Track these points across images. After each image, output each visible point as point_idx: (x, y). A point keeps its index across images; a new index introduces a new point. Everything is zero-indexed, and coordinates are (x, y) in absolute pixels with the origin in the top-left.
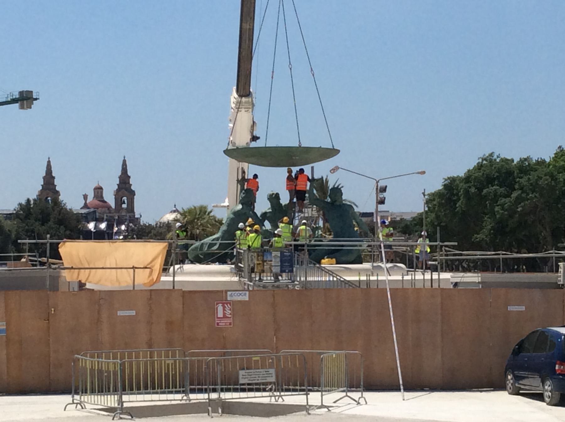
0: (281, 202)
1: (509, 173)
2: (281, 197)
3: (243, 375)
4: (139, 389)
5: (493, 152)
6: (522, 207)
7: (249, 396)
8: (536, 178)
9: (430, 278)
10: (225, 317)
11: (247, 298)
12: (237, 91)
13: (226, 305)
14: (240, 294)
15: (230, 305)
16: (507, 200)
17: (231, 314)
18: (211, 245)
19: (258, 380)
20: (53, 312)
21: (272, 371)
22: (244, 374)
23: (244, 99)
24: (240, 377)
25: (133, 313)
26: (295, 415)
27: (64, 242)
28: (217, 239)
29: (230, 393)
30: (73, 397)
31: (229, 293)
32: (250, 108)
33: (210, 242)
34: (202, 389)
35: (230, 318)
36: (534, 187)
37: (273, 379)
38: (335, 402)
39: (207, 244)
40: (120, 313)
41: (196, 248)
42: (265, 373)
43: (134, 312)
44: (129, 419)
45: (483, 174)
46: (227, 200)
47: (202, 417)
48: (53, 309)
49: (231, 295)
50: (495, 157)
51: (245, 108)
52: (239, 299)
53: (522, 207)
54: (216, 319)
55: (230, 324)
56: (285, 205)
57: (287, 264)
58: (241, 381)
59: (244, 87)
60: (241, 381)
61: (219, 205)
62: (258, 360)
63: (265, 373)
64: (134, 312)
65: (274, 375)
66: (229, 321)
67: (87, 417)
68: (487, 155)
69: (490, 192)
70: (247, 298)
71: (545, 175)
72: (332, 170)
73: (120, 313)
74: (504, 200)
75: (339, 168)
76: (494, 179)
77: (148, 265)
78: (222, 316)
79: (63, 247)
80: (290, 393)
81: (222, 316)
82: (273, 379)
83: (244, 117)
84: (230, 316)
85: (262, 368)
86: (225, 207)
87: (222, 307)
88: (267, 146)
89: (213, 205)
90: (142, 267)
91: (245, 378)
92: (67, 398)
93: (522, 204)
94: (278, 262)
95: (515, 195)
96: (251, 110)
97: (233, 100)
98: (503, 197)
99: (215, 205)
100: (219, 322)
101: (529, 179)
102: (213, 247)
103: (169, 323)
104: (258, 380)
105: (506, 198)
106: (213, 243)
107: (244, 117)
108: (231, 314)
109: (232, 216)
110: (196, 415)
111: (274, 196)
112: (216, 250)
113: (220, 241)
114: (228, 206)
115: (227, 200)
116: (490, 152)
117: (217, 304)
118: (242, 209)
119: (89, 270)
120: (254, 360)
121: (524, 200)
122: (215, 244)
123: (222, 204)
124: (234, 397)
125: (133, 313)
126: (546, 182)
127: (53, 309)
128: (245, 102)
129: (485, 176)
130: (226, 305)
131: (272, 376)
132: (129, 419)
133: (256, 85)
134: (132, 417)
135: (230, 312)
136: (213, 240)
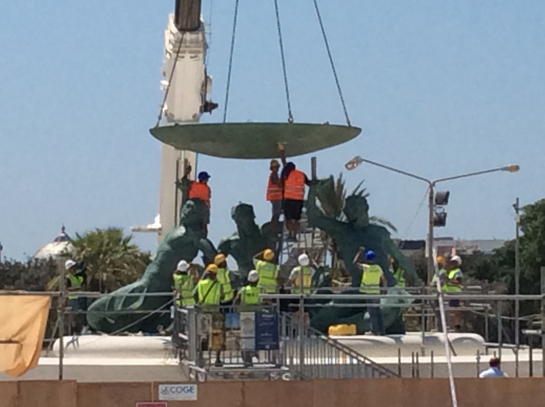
11: (193, 396)
12: (177, 22)
14: (183, 389)
18: (129, 300)
23: (188, 36)
28: (140, 289)
31: (161, 387)
32: (199, 52)
33: (127, 294)
39: (121, 297)
41: (103, 305)
46: (157, 219)
49: (165, 391)
51: (190, 52)
57: (267, 334)
61: (143, 227)
70: (193, 396)
72: (350, 163)
77: (15, 336)
83: (189, 69)
89: (132, 228)
94: (251, 332)
96: (201, 56)
107: (189, 69)
113: (144, 294)
114: (160, 229)
115: (157, 219)
118: (185, 234)
122: (137, 298)
123: (149, 227)
128: (191, 42)
136: (133, 291)
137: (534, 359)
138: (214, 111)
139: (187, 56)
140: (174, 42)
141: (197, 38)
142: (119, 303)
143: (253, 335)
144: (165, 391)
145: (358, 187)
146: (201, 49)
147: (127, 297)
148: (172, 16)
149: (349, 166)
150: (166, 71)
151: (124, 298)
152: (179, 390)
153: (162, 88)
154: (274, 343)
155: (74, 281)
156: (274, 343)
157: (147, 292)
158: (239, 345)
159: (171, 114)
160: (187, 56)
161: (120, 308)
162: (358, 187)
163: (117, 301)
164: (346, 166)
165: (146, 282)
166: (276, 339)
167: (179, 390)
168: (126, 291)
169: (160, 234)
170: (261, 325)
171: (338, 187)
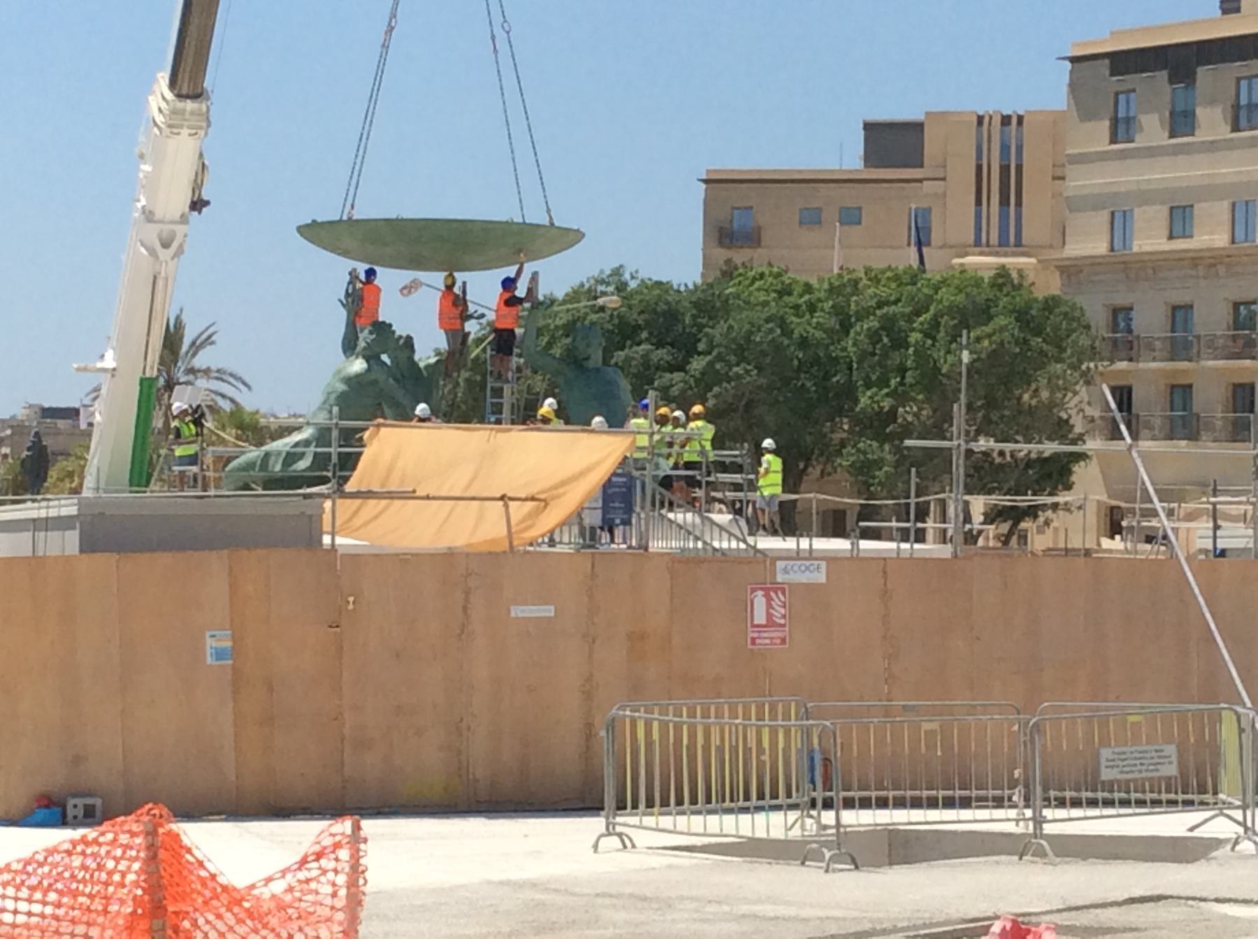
0: (416, 358)
1: (672, 315)
2: (416, 347)
3: (1108, 760)
4: (680, 802)
5: (621, 266)
6: (715, 396)
7: (962, 818)
8: (747, 327)
9: (807, 547)
10: (770, 622)
11: (822, 578)
12: (173, 84)
13: (772, 594)
14: (807, 568)
15: (784, 594)
16: (678, 376)
17: (784, 617)
18: (291, 458)
19: (1140, 771)
20: (351, 607)
21: (1171, 750)
22: (1111, 757)
23: (190, 105)
24: (1103, 763)
25: (548, 611)
26: (945, 865)
27: (379, 426)
28: (307, 443)
29: (854, 812)
30: (607, 818)
31: (780, 565)
32: (200, 128)
33: (287, 449)
34: (853, 799)
35: (784, 626)
36: (742, 350)
37: (1171, 770)
38: (1191, 829)
39: (279, 453)
40: (517, 612)
41: (250, 466)
42: (1154, 754)
43: (552, 608)
44: (849, 870)
45: (612, 316)
46: (110, 354)
47: (997, 863)
48: (351, 599)
49: (785, 571)
50: (627, 276)
51: (189, 127)
52: (805, 581)
53: (715, 396)
54: (750, 629)
55: (783, 641)
56: (428, 367)
57: (617, 505)
58: (1106, 775)
59: (188, 71)
60: (1106, 775)
61: (91, 365)
62: (1139, 723)
63: (1154, 754)
64: (552, 608)
65: (1174, 759)
66: (780, 634)
67: (697, 865)
68: (608, 272)
69: (633, 358)
70: (822, 578)
71: (767, 321)
72: (405, 288)
73: (517, 612)
74: (668, 375)
75: (422, 284)
76: (637, 328)
77: (543, 492)
78: (763, 622)
79: (375, 442)
80: (1129, 811)
81: (763, 622)
82: (1171, 770)
83: (183, 148)
84: (782, 621)
85: (1147, 743)
86: (104, 370)
87: (764, 599)
88: (357, 216)
89: (75, 366)
90: (523, 496)
91: (1112, 767)
92: (593, 825)
93: (716, 389)
94: (596, 501)
95: (697, 364)
96: (202, 133)
97: (154, 102)
98: (664, 371)
99: (83, 365)
100: (756, 635)
101: (730, 327)
102: (295, 462)
103: (636, 638)
104: (1140, 771)
105: (671, 372)
106: (295, 454)
107: (183, 148)
108: (784, 617)
109: (342, 387)
110: (963, 860)
111: (402, 342)
112: (304, 471)
113: (312, 449)
114: (114, 369)
115: (110, 354)
116: (617, 265)
117: (753, 590)
118: (369, 370)
119: (452, 502)
120: (1132, 723)
121: (719, 379)
122: (302, 455)
123: (99, 365)
124: (913, 820)
125: (548, 611)
126: (770, 337)
127: (351, 599)
128: (192, 113)
129: (616, 321)
130: (772, 594)
131: (1171, 763)
132: (849, 870)
133: (218, 74)
134: (857, 867)
135: (783, 611)
136: (297, 445)
137: (801, 547)
138: (204, 210)
139: (185, 132)
140: (166, 112)
141: (200, 109)
142: (276, 462)
143: (600, 505)
144: (785, 571)
145: (207, 329)
146: (204, 124)
147: (288, 453)
148: (163, 78)
149: (405, 292)
150: (144, 151)
151: (284, 455)
152: (796, 568)
153: (141, 175)
154: (625, 516)
155: (185, 431)
156: (625, 516)
157: (317, 446)
158: (581, 519)
159: (150, 212)
160: (185, 132)
161: (278, 468)
162: (207, 329)
163: (273, 458)
164: (401, 291)
165: (312, 435)
166: (629, 510)
167: (796, 568)
168: (286, 445)
169: (113, 376)
170: (610, 491)
171: (175, 326)
